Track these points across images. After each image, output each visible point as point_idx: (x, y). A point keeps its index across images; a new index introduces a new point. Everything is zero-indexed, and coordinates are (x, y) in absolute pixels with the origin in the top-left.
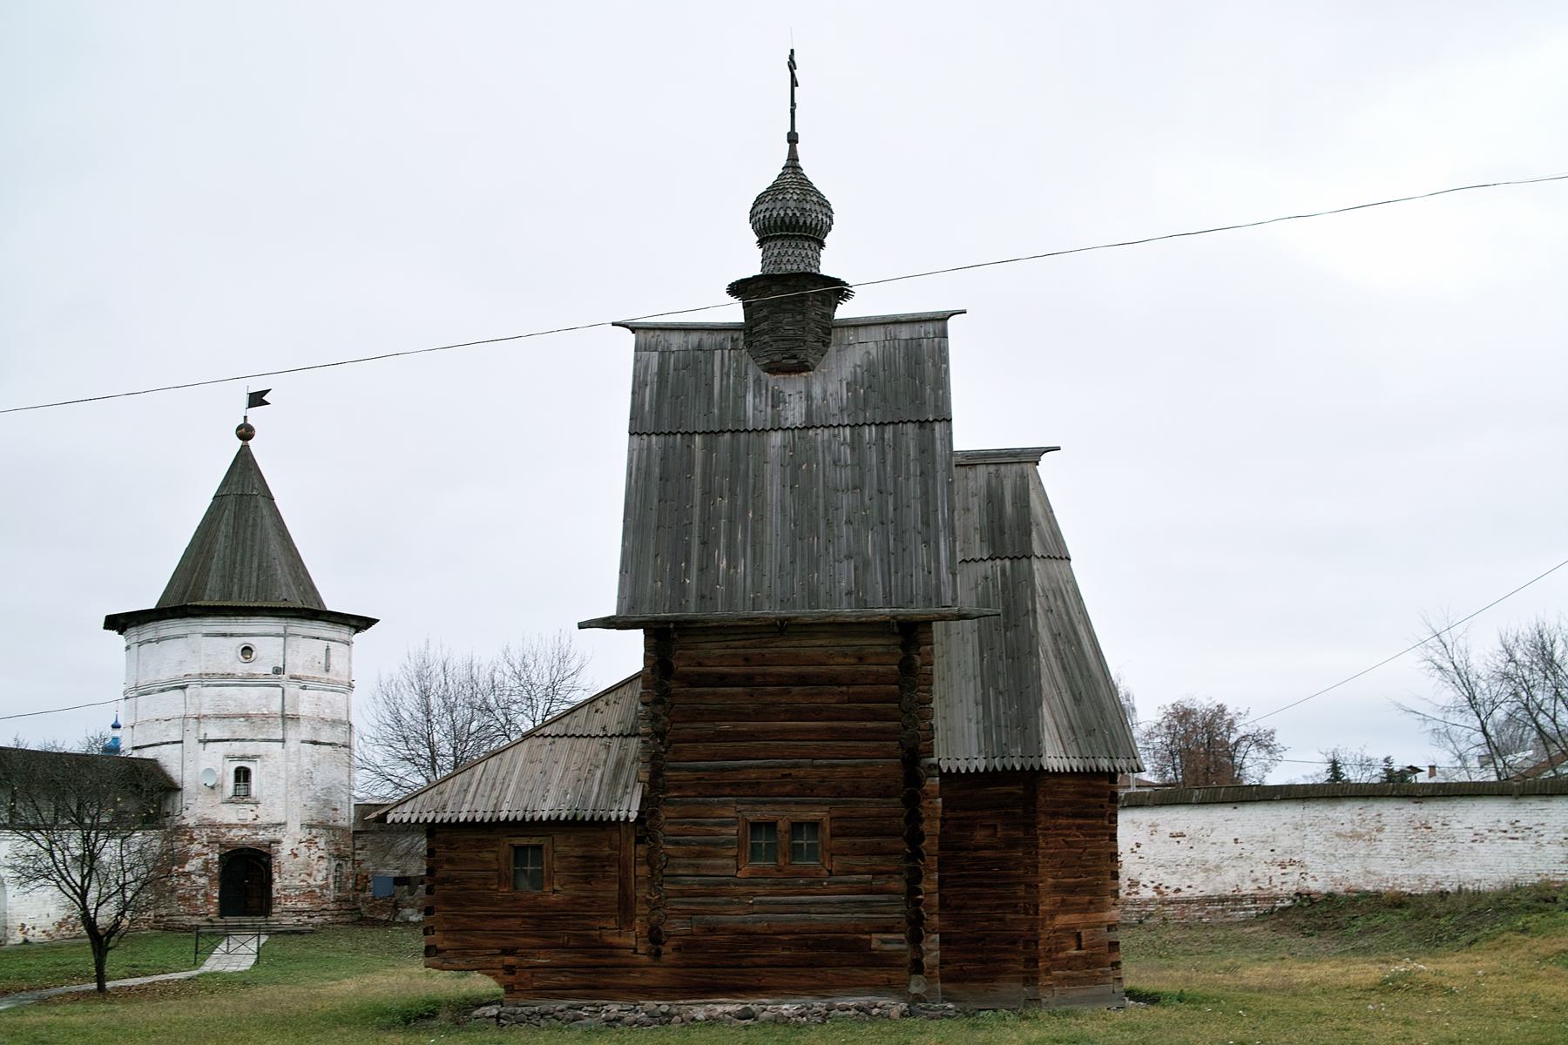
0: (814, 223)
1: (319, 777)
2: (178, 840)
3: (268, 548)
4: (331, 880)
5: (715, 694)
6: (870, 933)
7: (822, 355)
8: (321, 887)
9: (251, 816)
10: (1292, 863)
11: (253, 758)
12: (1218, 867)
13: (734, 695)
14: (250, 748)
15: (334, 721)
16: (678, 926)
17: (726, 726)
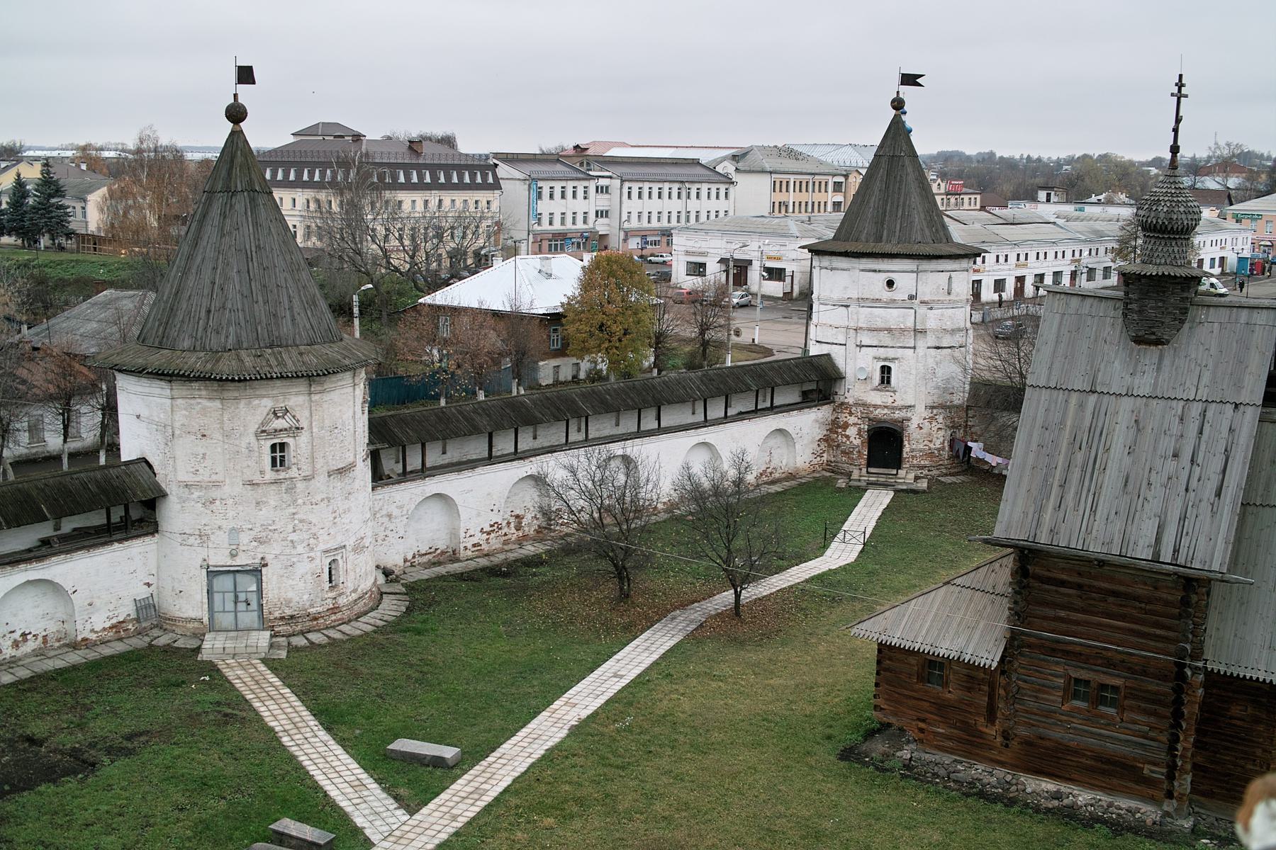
0: (1180, 228)
1: (940, 372)
2: (842, 412)
3: (910, 200)
4: (946, 444)
5: (1056, 591)
6: (1144, 764)
7: (1178, 331)
8: (939, 450)
9: (891, 400)
13: (1069, 595)
14: (891, 353)
15: (953, 330)
16: (1022, 731)
17: (1062, 614)
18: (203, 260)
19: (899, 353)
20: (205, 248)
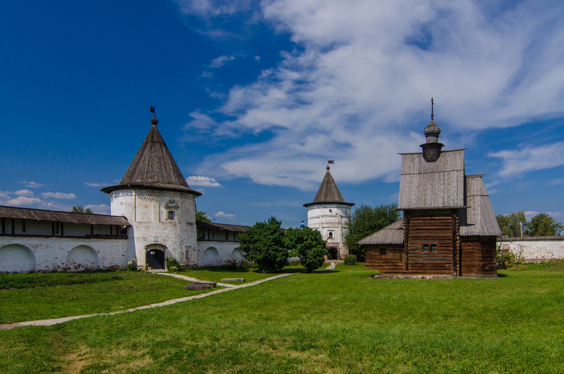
10: (550, 252)
11: (333, 231)
12: (533, 253)
17: (419, 228)
18: (145, 159)
19: (334, 229)
20: (145, 156)
